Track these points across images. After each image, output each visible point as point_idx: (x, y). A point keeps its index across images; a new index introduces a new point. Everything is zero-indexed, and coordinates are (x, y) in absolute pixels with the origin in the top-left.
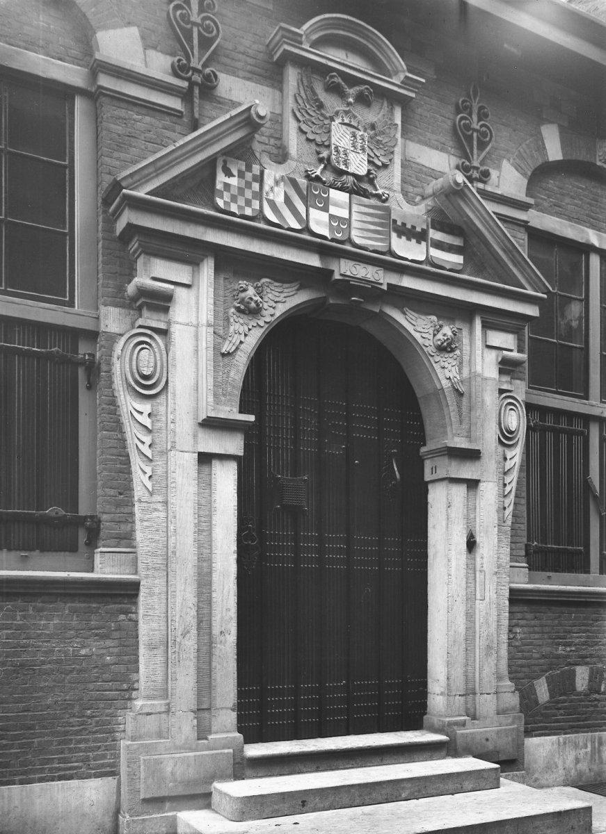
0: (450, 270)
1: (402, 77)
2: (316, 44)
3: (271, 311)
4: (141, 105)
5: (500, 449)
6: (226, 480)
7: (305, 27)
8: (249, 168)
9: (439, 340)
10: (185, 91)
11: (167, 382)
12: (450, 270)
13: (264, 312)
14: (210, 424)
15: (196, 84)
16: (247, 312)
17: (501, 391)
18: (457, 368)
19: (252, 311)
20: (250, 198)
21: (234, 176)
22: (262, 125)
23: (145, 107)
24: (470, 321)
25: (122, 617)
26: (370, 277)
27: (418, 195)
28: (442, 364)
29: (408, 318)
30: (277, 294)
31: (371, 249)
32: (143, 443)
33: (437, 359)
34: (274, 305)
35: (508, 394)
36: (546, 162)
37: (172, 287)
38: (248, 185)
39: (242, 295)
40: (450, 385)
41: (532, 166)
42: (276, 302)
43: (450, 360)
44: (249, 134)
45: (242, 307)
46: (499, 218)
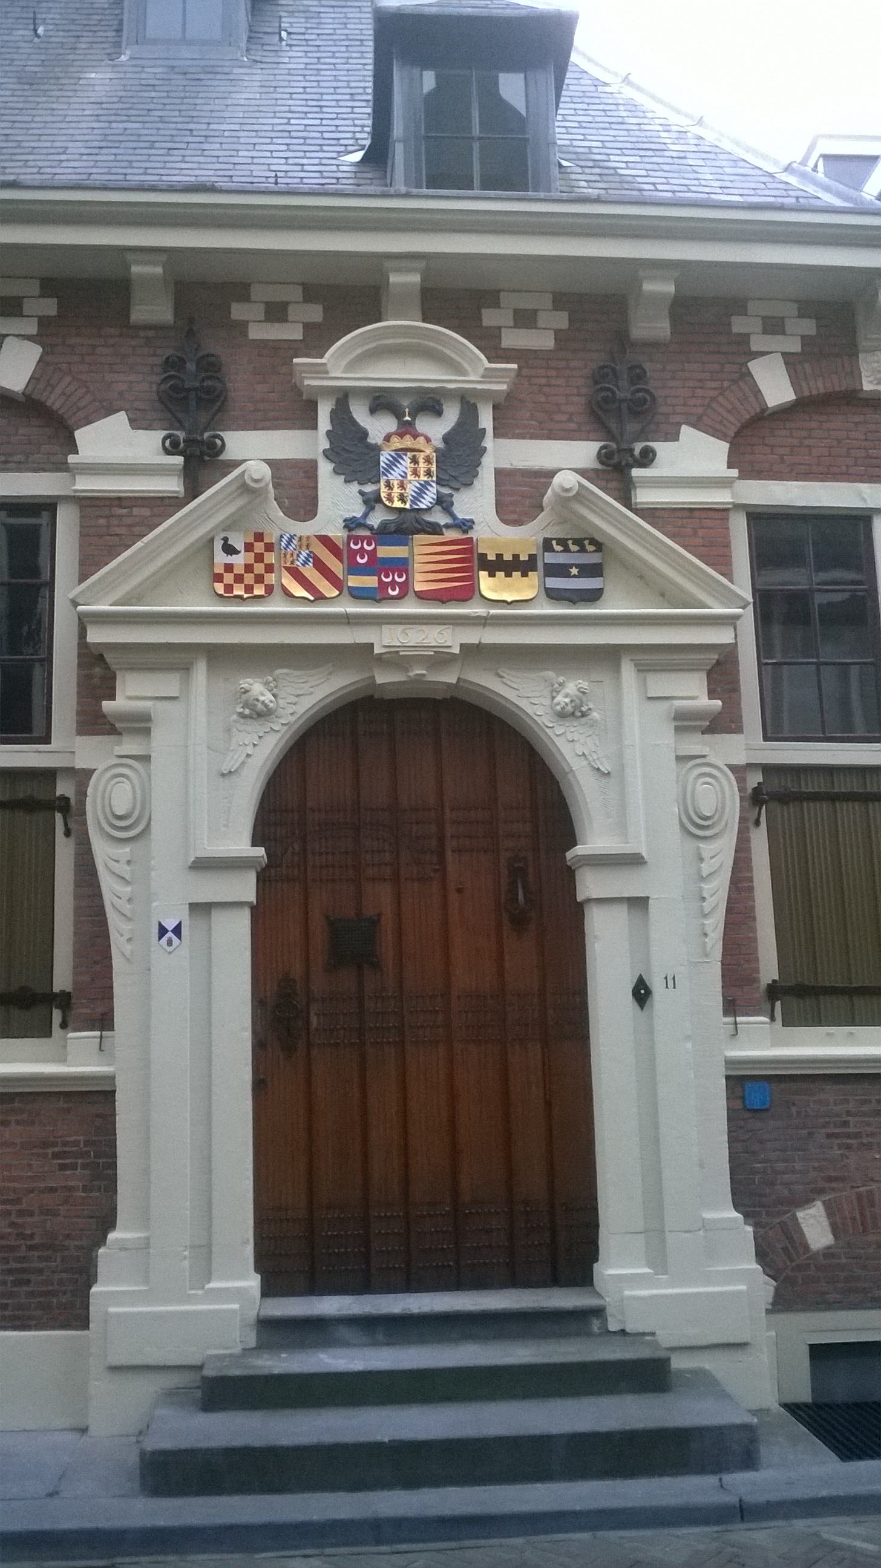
5: (691, 845)
7: (327, 355)
9: (558, 704)
14: (203, 865)
17: (681, 759)
19: (260, 714)
21: (237, 552)
24: (617, 669)
28: (570, 737)
34: (295, 699)
35: (699, 761)
39: (244, 697)
44: (249, 503)
45: (247, 712)
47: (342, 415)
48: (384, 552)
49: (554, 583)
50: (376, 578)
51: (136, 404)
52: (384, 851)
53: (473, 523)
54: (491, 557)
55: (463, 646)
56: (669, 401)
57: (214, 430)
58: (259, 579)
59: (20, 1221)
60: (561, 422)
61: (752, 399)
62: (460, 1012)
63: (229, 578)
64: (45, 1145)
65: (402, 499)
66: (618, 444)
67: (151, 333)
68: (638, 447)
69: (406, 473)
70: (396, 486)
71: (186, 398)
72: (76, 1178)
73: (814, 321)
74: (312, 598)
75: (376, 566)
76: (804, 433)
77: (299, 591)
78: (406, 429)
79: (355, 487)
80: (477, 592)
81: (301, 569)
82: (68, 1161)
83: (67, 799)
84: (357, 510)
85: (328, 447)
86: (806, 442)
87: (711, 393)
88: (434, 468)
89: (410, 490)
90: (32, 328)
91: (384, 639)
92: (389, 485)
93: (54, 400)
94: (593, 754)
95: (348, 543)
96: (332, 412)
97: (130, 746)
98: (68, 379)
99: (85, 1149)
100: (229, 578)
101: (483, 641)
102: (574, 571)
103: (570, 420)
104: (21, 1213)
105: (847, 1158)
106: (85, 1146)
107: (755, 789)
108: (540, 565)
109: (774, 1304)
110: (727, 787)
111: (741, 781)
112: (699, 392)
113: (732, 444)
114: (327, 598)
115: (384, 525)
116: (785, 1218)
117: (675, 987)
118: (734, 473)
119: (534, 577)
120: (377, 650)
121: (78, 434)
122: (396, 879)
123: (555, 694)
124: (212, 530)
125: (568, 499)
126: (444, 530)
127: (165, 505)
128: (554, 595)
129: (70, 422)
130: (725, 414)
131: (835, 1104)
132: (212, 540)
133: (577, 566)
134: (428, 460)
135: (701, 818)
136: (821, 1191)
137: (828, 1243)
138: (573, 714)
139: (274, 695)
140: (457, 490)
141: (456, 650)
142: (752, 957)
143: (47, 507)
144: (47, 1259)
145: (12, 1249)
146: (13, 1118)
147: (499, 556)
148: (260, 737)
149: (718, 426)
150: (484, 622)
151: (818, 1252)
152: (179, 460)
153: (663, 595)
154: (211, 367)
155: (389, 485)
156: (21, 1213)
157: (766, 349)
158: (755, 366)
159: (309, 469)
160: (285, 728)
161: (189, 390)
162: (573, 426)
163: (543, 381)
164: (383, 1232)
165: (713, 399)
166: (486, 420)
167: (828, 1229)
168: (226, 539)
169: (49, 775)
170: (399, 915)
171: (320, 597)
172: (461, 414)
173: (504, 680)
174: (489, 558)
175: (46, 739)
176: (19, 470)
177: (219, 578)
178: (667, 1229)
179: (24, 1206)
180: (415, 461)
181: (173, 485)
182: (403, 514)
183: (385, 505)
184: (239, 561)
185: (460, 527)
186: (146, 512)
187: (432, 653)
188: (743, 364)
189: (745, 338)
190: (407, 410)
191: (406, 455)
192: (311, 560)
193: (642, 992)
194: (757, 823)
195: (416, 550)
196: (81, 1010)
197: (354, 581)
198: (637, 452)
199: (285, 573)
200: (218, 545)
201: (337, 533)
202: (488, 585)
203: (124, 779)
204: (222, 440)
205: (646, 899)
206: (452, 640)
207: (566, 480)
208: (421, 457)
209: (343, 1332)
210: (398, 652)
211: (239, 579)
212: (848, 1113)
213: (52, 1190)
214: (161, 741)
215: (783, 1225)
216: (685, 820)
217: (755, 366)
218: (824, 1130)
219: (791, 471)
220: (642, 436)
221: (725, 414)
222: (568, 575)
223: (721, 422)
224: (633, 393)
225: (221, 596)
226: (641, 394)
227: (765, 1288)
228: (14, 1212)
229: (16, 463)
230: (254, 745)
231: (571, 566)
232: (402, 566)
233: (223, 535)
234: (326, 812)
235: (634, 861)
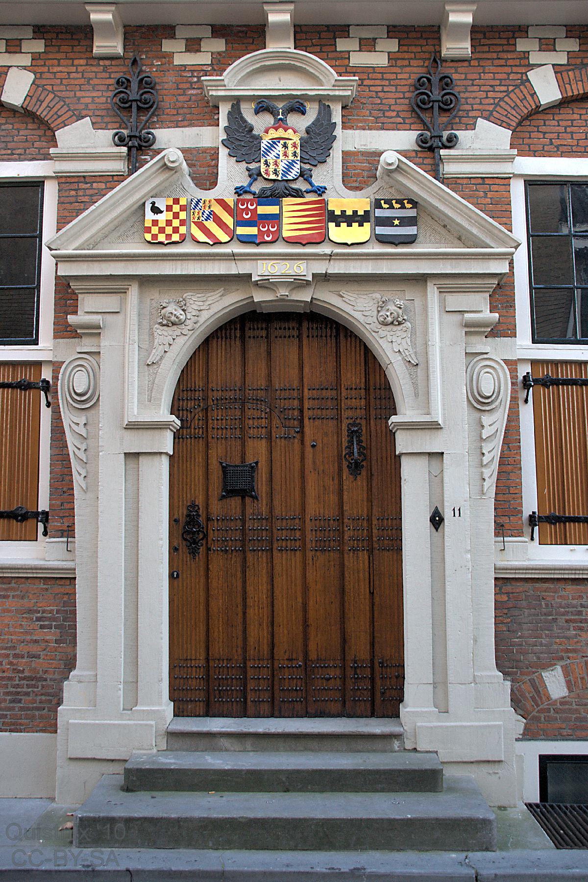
2: (243, 80)
7: (225, 73)
16: (170, 325)
18: (409, 340)
21: (162, 212)
29: (347, 301)
30: (201, 303)
32: (79, 449)
33: (382, 333)
35: (485, 356)
37: (99, 317)
43: (399, 333)
45: (165, 322)
47: (235, 115)
48: (262, 210)
49: (380, 230)
50: (256, 228)
51: (97, 113)
52: (262, 418)
53: (326, 189)
54: (338, 213)
57: (149, 128)
58: (176, 230)
59: (15, 661)
60: (392, 117)
61: (529, 98)
62: (312, 530)
63: (155, 230)
64: (30, 611)
65: (276, 172)
66: (431, 132)
67: (107, 62)
68: (445, 134)
69: (279, 155)
70: (272, 164)
71: (131, 107)
72: (51, 635)
73: (578, 40)
74: (211, 243)
75: (257, 220)
76: (569, 123)
77: (202, 237)
78: (280, 124)
79: (244, 165)
80: (327, 238)
81: (205, 222)
82: (46, 623)
83: (48, 382)
84: (244, 181)
85: (225, 138)
86: (569, 130)
87: (501, 95)
88: (298, 151)
89: (282, 166)
90: (26, 60)
91: (262, 269)
92: (266, 163)
93: (42, 111)
94: (406, 351)
95: (237, 205)
96: (229, 113)
97: (87, 345)
98: (51, 96)
99: (57, 615)
100: (155, 230)
101: (329, 272)
102: (396, 222)
103: (398, 116)
104: (16, 656)
105: (580, 636)
106: (57, 613)
107: (524, 377)
108: (372, 219)
109: (524, 734)
110: (501, 375)
111: (513, 372)
112: (491, 94)
113: (514, 131)
114: (221, 243)
115: (263, 190)
116: (534, 676)
117: (460, 516)
118: (515, 152)
119: (367, 225)
121: (56, 133)
122: (269, 438)
123: (379, 309)
124: (145, 196)
125: (391, 171)
126: (305, 193)
127: (115, 179)
128: (382, 240)
130: (509, 109)
131: (573, 599)
132: (144, 204)
133: (398, 218)
134: (294, 146)
135: (482, 397)
136: (562, 658)
137: (564, 695)
138: (392, 323)
139: (184, 310)
140: (315, 166)
142: (518, 495)
143: (36, 185)
144: (34, 686)
145: (10, 679)
146: (11, 594)
147: (343, 212)
148: (174, 339)
149: (505, 119)
150: (330, 257)
151: (556, 701)
152: (124, 149)
153: (459, 239)
154: (146, 84)
155: (266, 163)
156: (16, 656)
157: (543, 63)
158: (531, 75)
159: (214, 154)
160: (191, 332)
161: (132, 101)
162: (400, 120)
163: (380, 89)
164: (184, 699)
165: (501, 99)
166: (337, 117)
167: (564, 684)
168: (153, 203)
169: (37, 365)
170: (271, 461)
171: (218, 243)
172: (319, 113)
174: (336, 213)
175: (36, 342)
176: (20, 160)
177: (148, 230)
178: (451, 678)
179: (17, 651)
180: (285, 146)
181: (119, 166)
182: (276, 183)
183: (263, 177)
184: (162, 218)
185: (316, 192)
186: (103, 186)
187: (293, 280)
188: (524, 73)
189: (526, 55)
190: (281, 111)
191: (279, 142)
192: (212, 216)
193: (437, 519)
194: (526, 401)
195: (285, 208)
196: (53, 524)
197: (241, 231)
198: (444, 139)
199: (193, 225)
200: (148, 207)
201: (230, 200)
202: (339, 233)
203: (83, 369)
204: (152, 134)
205: (443, 453)
206: (303, 269)
207: (390, 158)
208: (290, 143)
209: (224, 742)
211: (162, 230)
212: (582, 606)
213: (36, 641)
214: (106, 343)
215: (532, 682)
216: (471, 399)
217: (531, 75)
218: (564, 617)
219: (558, 150)
220: (450, 125)
221: (509, 109)
222: (392, 225)
223: (506, 116)
224: (442, 97)
225: (149, 242)
226: (447, 97)
227: (518, 724)
228: (11, 655)
229: (18, 154)
230: (170, 345)
231: (394, 218)
232: (276, 219)
233: (151, 200)
234: (222, 391)
235: (434, 426)
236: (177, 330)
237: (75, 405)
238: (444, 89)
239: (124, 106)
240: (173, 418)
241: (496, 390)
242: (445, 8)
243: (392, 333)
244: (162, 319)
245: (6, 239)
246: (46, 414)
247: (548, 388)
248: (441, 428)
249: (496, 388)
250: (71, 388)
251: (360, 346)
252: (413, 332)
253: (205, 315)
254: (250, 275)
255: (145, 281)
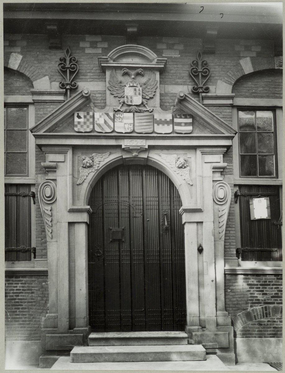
0: (185, 134)
1: (156, 60)
3: (98, 165)
4: (211, 106)
6: (81, 232)
8: (88, 114)
10: (64, 92)
11: (227, 201)
12: (185, 134)
13: (94, 167)
15: (68, 89)
20: (89, 125)
22: (90, 95)
23: (51, 102)
25: (44, 284)
26: (139, 144)
27: (171, 106)
30: (100, 158)
31: (144, 133)
32: (49, 221)
36: (243, 75)
37: (55, 163)
38: (88, 120)
39: (84, 161)
40: (185, 182)
41: (234, 79)
42: (100, 162)
46: (205, 106)
55: (149, 146)
56: (231, 221)
88: (141, 93)
120: (123, 147)
121: (34, 83)
123: (176, 161)
129: (32, 79)
141: (147, 147)
168: (78, 114)
173: (161, 157)
184: (82, 120)
187: (140, 148)
200: (76, 115)
208: (137, 89)
210: (129, 148)
222: (181, 126)
236: (90, 170)
237: (46, 202)
238: (203, 67)
239: (63, 71)
240: (89, 207)
241: (225, 196)
242: (193, 121)
243: (181, 172)
244: (83, 165)
245: (11, 131)
246: (33, 207)
247: (246, 197)
248: (203, 212)
249: (225, 195)
250: (44, 194)
251: (167, 180)
252: (190, 171)
253: (102, 164)
254: (121, 146)
255: (75, 148)
